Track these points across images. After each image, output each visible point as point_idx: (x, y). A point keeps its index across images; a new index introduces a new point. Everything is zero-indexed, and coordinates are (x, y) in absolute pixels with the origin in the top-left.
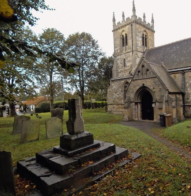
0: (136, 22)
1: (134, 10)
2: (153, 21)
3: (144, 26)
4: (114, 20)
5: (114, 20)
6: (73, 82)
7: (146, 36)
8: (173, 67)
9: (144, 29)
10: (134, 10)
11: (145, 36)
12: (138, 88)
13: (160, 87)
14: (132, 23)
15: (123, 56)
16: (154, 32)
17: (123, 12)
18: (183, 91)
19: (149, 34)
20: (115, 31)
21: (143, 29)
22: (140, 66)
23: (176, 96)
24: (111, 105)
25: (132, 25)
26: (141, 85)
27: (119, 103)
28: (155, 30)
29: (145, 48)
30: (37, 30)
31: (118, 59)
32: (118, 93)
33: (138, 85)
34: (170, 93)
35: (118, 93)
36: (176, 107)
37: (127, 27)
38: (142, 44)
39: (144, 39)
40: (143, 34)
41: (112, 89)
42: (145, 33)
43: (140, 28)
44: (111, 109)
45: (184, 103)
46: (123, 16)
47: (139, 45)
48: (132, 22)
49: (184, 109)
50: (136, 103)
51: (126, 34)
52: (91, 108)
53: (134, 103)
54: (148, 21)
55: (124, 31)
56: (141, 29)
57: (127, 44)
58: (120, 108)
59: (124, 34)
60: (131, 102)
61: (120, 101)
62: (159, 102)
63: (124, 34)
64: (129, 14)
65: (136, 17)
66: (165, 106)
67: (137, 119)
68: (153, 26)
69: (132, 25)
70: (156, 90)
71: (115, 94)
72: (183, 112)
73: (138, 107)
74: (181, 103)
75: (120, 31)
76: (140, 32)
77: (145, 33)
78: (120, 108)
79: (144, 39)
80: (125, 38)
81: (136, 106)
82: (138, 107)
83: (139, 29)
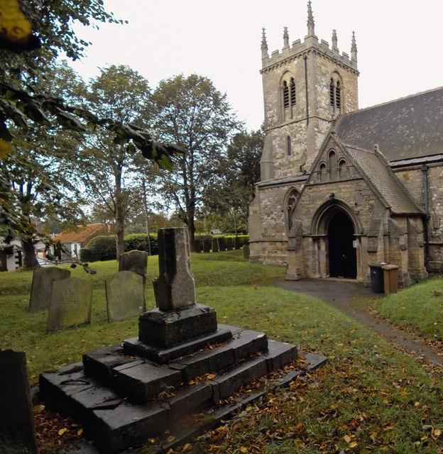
0: (315, 50)
1: (311, 23)
2: (354, 49)
3: (334, 61)
4: (264, 46)
5: (264, 46)
6: (170, 190)
7: (338, 83)
8: (402, 155)
9: (335, 67)
10: (311, 23)
11: (335, 84)
12: (320, 203)
13: (371, 202)
14: (306, 54)
15: (286, 131)
16: (357, 73)
17: (286, 28)
18: (424, 212)
19: (345, 79)
20: (267, 72)
21: (331, 67)
22: (325, 153)
23: (408, 223)
24: (257, 244)
25: (306, 59)
26: (327, 197)
27: (276, 238)
28: (359, 69)
29: (337, 112)
30: (87, 70)
31: (275, 137)
32: (273, 216)
33: (320, 198)
34: (394, 215)
35: (273, 216)
36: (409, 247)
37: (296, 62)
38: (328, 101)
39: (335, 90)
40: (332, 79)
41: (260, 207)
42: (336, 77)
43: (324, 65)
44: (258, 252)
45: (426, 238)
46: (286, 37)
47: (323, 104)
48: (306, 51)
49: (427, 252)
50: (316, 240)
51: (292, 79)
52: (211, 251)
53: (311, 240)
54: (344, 48)
55: (287, 71)
56: (327, 67)
57: (293, 103)
58: (278, 249)
59: (287, 78)
60: (304, 237)
61: (278, 234)
62: (369, 237)
63: (287, 78)
64: (299, 33)
65: (316, 38)
66: (383, 247)
67: (317, 276)
68: (354, 61)
69: (306, 59)
70: (361, 208)
71: (266, 217)
72: (425, 259)
73: (319, 248)
74: (420, 238)
75: (279, 71)
76: (324, 75)
77: (336, 77)
78: (278, 249)
79: (335, 90)
80: (289, 88)
81: (316, 247)
82: (319, 248)
83: (323, 67)
